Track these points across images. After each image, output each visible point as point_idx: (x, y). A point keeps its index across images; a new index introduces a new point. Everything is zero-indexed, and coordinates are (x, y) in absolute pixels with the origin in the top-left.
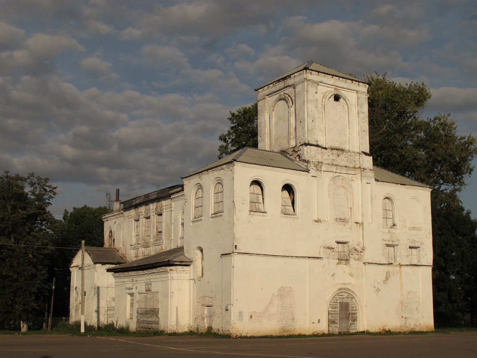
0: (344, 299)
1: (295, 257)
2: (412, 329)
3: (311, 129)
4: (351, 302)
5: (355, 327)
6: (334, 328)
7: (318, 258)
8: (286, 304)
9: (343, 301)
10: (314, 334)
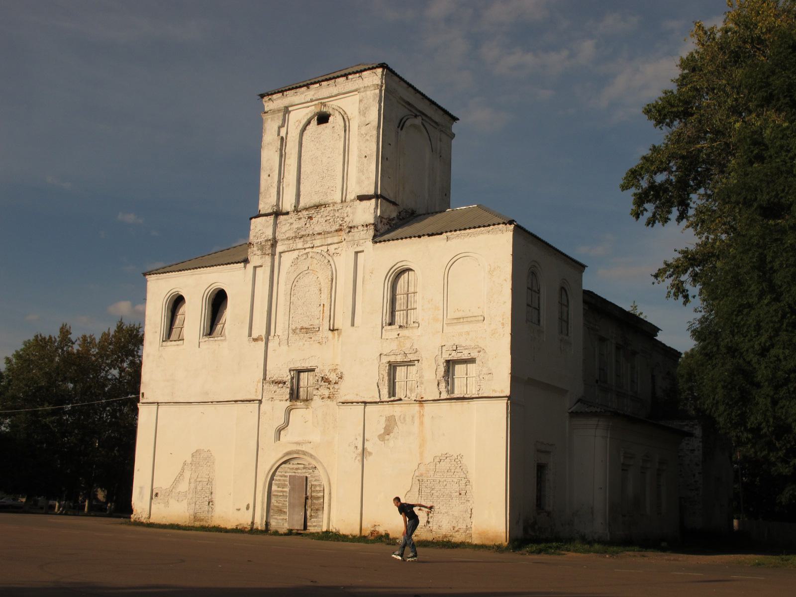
0: (299, 471)
1: (216, 403)
2: (445, 536)
3: (265, 190)
4: (312, 477)
5: (320, 522)
6: (280, 521)
7: (250, 401)
8: (201, 478)
9: (297, 474)
10: (239, 528)
